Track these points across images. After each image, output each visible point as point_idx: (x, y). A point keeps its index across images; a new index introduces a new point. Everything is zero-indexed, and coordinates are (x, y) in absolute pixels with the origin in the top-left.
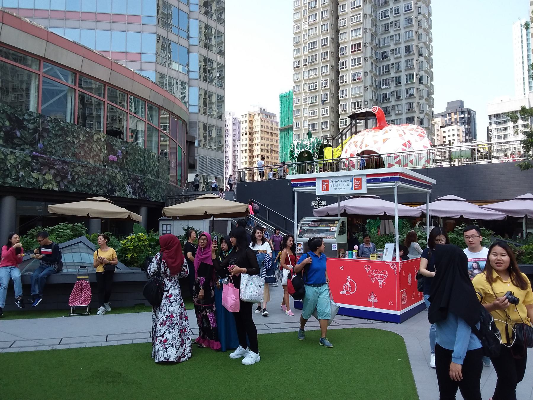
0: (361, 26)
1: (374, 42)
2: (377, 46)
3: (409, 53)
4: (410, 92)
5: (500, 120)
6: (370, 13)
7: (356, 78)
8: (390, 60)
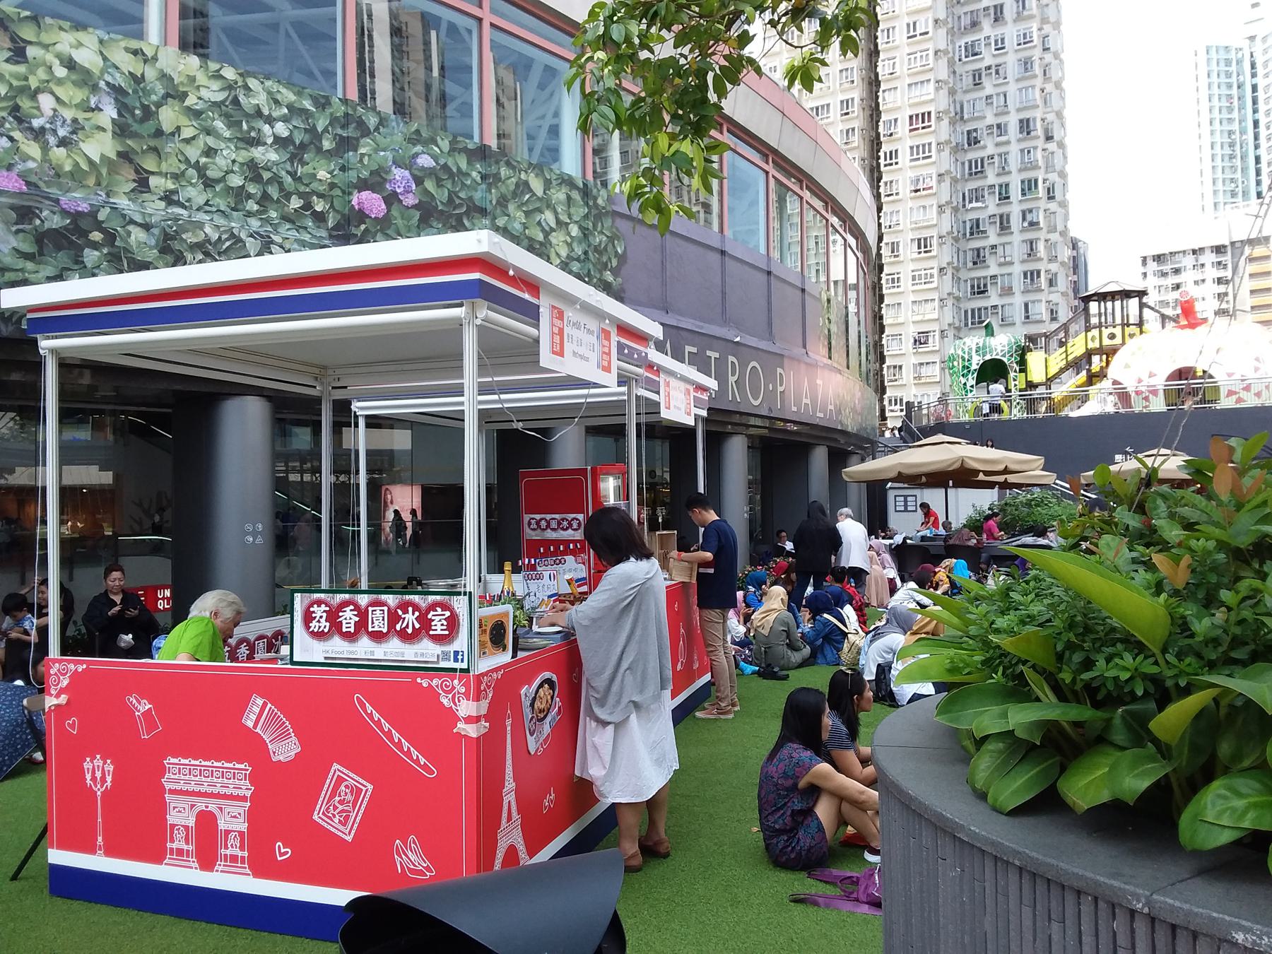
0: (931, 76)
1: (952, 109)
2: (959, 117)
3: (1028, 133)
4: (1029, 217)
5: (1167, 268)
7: (920, 186)
8: (984, 147)
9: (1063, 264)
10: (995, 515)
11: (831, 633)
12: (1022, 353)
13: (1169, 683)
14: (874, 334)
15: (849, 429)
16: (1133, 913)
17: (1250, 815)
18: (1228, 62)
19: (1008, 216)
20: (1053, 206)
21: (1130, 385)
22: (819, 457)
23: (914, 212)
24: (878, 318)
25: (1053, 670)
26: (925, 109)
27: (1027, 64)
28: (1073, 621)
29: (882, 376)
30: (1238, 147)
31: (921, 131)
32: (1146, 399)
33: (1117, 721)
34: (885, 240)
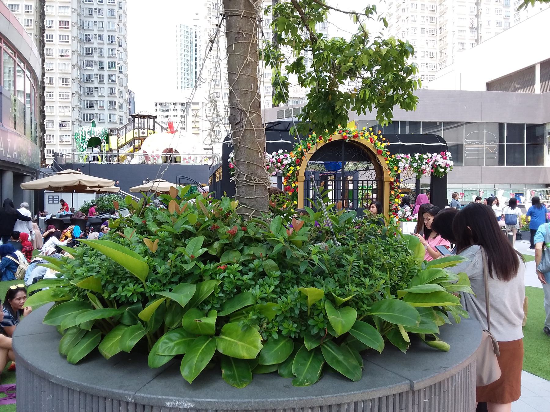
1: (79, 23)
2: (82, 27)
3: (112, 42)
4: (111, 78)
5: (164, 108)
7: (63, 54)
9: (125, 100)
10: (95, 205)
11: (10, 264)
12: (108, 136)
13: (147, 295)
14: (40, 119)
15: (25, 164)
16: (128, 403)
17: (176, 348)
18: (188, 33)
19: (103, 76)
20: (121, 75)
21: (150, 153)
22: (9, 178)
23: (60, 66)
24: (42, 112)
25: (99, 292)
26: (67, 20)
27: (112, 12)
28: (109, 270)
29: (44, 139)
30: (189, 67)
31: (64, 29)
32: (155, 159)
33: (126, 314)
34: (46, 75)
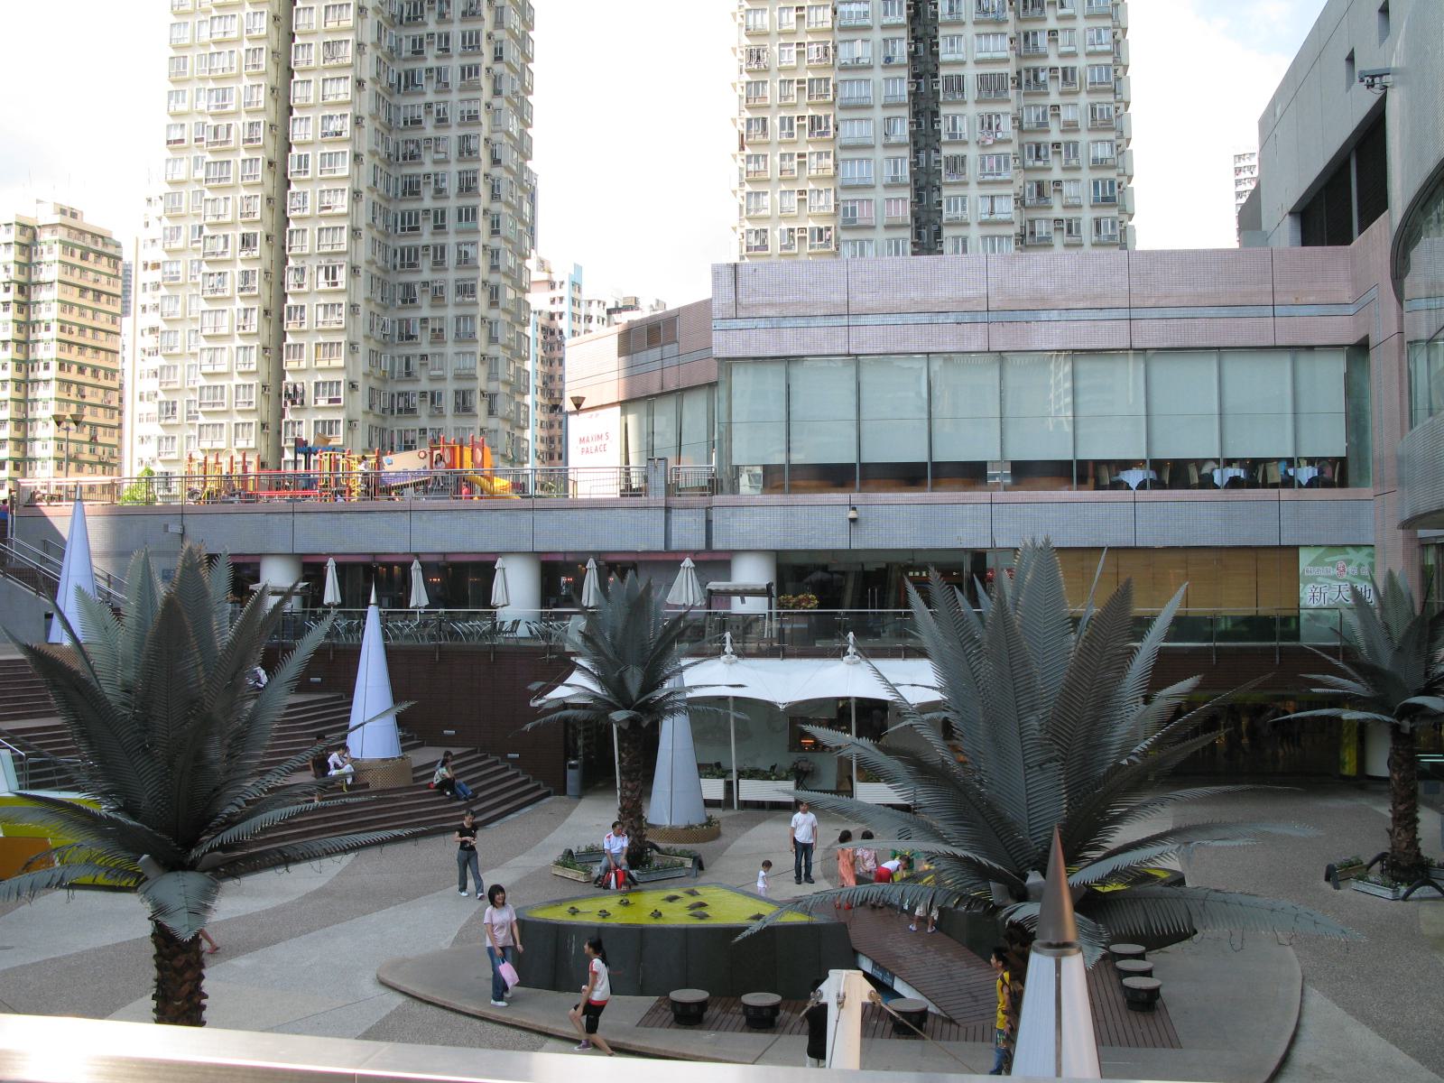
1: (380, 186)
6: (375, 38)
